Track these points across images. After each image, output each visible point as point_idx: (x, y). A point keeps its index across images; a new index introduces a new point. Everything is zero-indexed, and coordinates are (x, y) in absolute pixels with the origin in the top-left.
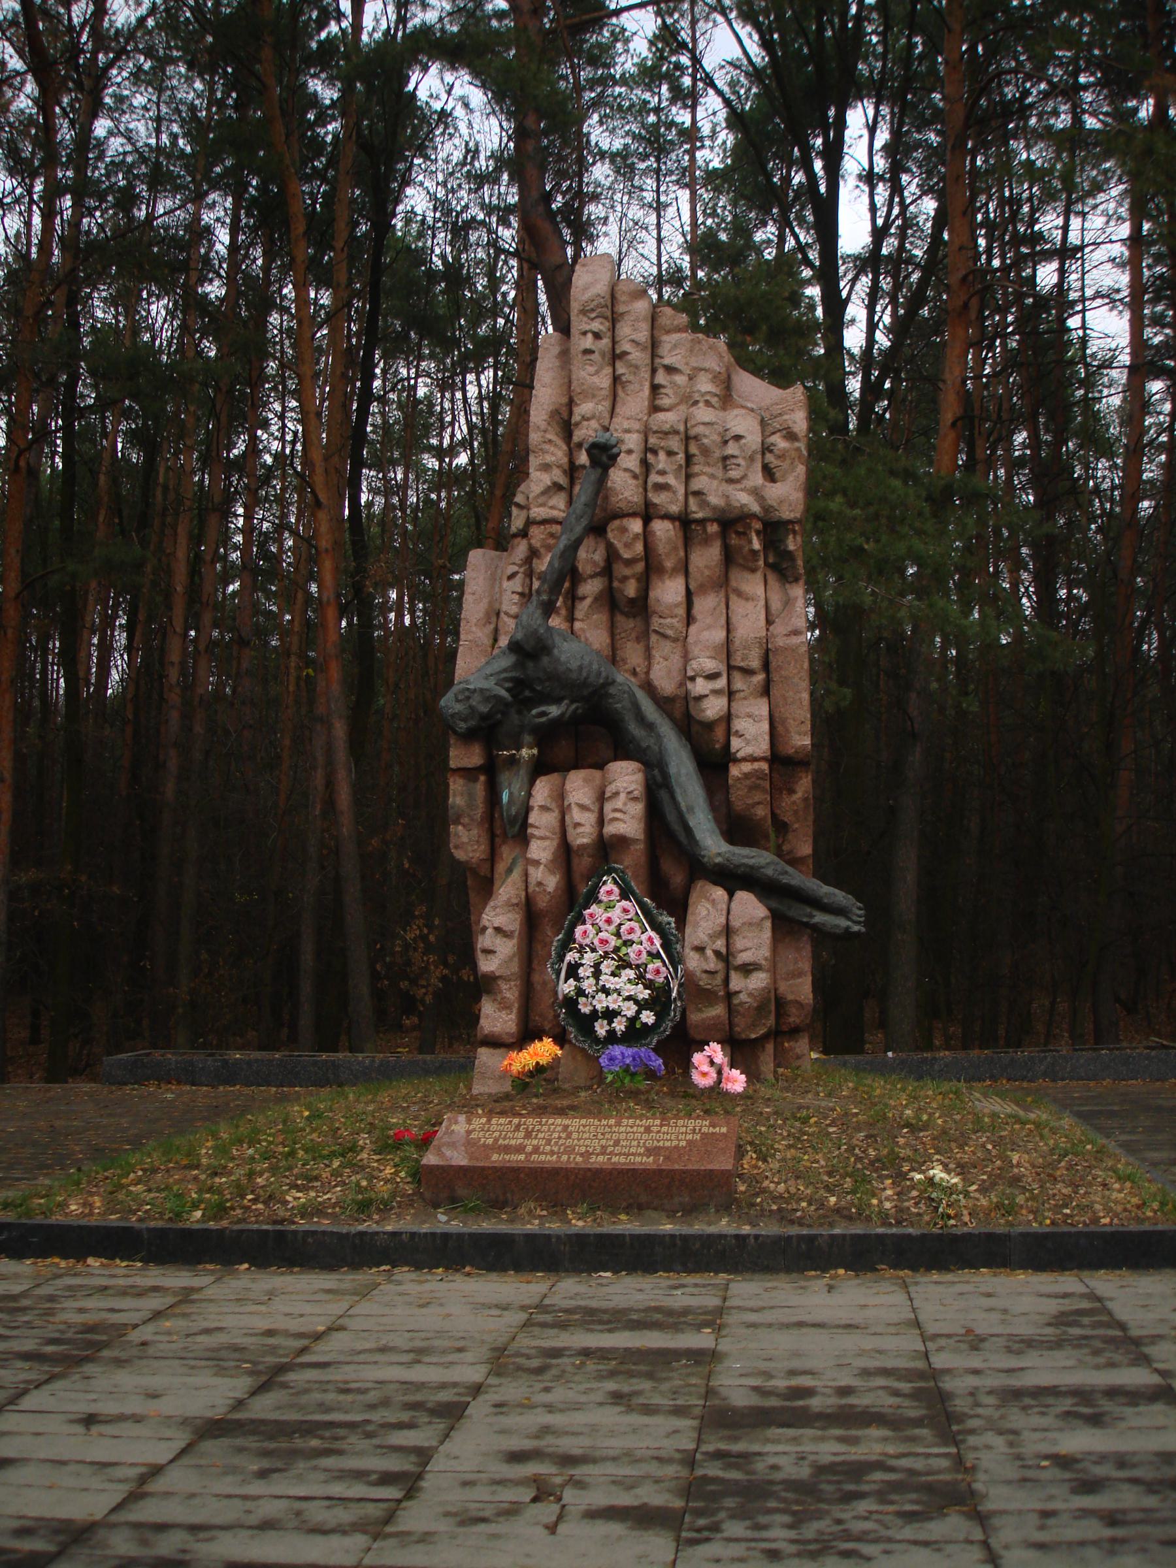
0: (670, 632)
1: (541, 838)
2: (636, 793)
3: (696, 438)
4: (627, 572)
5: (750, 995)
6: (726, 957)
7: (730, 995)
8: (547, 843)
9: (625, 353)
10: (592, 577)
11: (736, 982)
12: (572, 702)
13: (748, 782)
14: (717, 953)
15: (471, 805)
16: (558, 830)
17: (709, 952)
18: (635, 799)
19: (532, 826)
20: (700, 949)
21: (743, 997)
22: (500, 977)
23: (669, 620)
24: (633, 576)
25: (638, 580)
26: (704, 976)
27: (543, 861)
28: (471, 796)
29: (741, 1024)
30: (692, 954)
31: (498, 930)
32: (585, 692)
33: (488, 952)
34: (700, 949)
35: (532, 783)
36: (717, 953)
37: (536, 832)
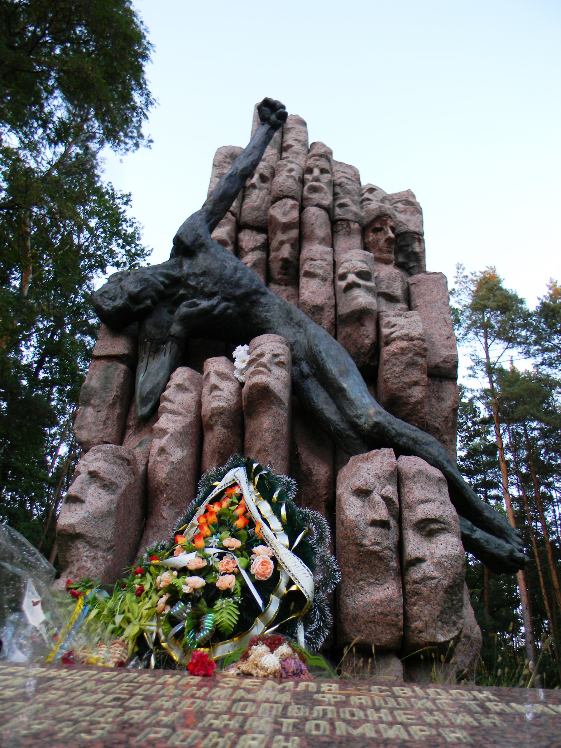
0: (320, 272)
1: (173, 412)
2: (282, 358)
3: (340, 185)
4: (284, 237)
5: (439, 564)
6: (397, 509)
7: (406, 565)
8: (179, 418)
9: (290, 146)
10: (253, 250)
11: (415, 545)
12: (225, 299)
13: (405, 359)
14: (387, 500)
15: (105, 388)
16: (193, 408)
17: (376, 496)
18: (280, 364)
19: (166, 399)
20: (363, 493)
21: (427, 568)
22: (78, 536)
23: (319, 262)
24: (289, 240)
25: (292, 245)
26: (371, 530)
27: (171, 430)
28: (107, 379)
29: (423, 612)
30: (353, 499)
31: (93, 475)
32: (238, 292)
33: (74, 500)
34: (363, 493)
35: (172, 369)
36: (387, 500)
37: (168, 405)
